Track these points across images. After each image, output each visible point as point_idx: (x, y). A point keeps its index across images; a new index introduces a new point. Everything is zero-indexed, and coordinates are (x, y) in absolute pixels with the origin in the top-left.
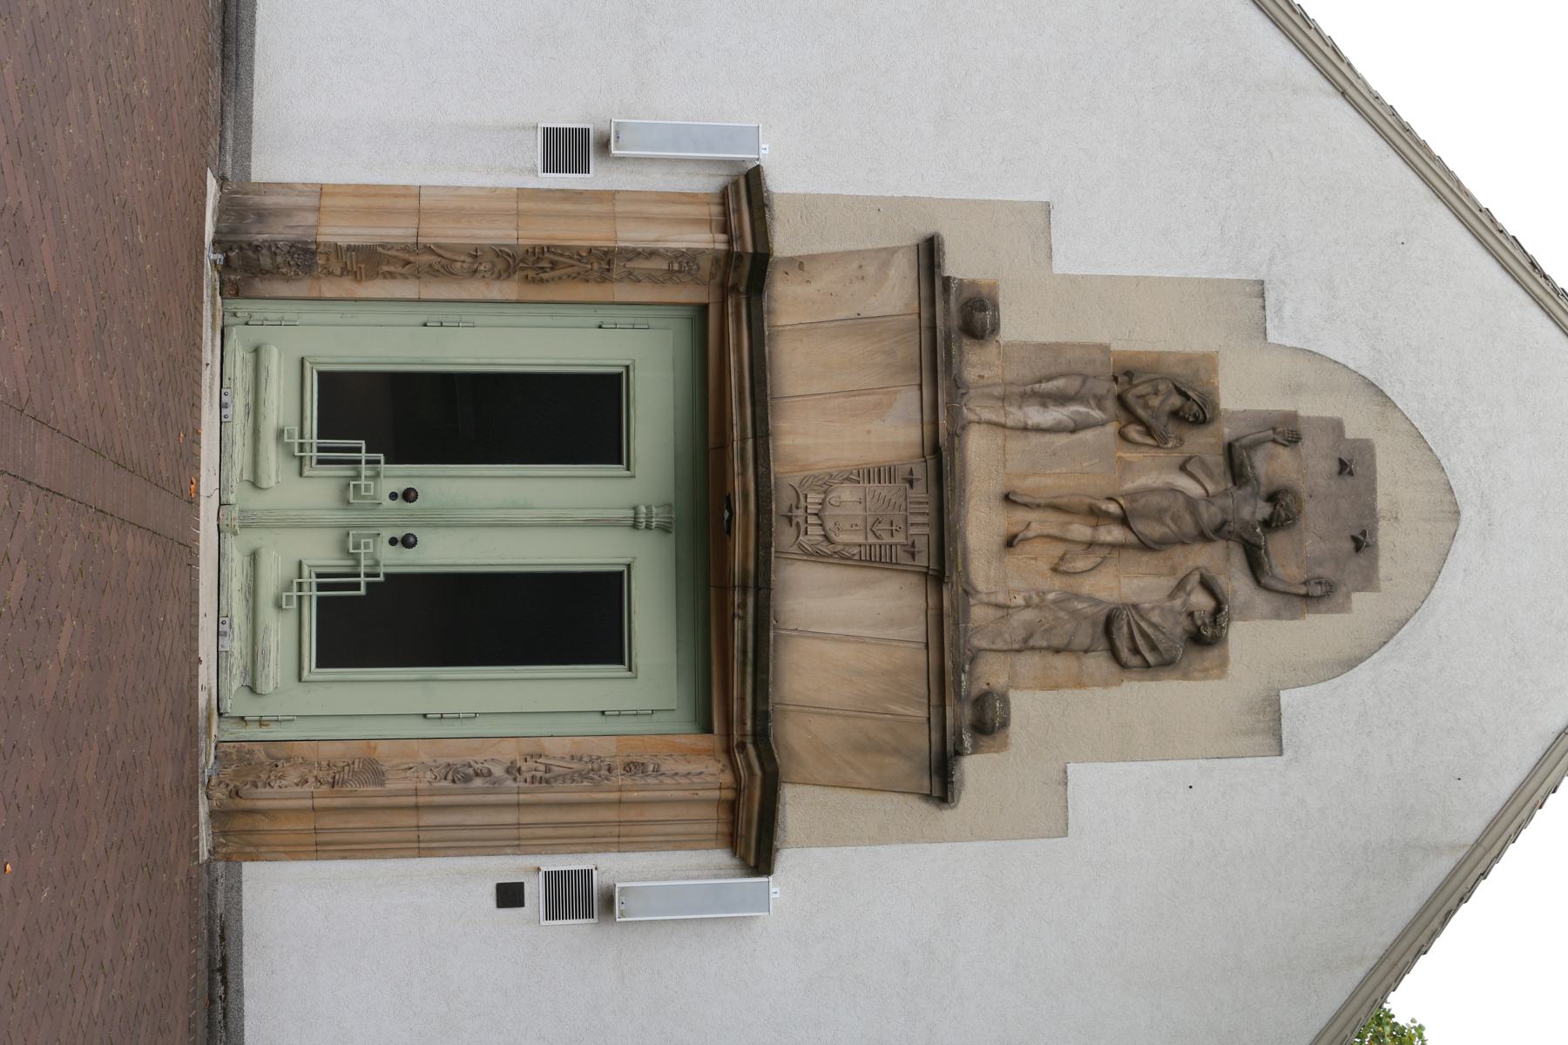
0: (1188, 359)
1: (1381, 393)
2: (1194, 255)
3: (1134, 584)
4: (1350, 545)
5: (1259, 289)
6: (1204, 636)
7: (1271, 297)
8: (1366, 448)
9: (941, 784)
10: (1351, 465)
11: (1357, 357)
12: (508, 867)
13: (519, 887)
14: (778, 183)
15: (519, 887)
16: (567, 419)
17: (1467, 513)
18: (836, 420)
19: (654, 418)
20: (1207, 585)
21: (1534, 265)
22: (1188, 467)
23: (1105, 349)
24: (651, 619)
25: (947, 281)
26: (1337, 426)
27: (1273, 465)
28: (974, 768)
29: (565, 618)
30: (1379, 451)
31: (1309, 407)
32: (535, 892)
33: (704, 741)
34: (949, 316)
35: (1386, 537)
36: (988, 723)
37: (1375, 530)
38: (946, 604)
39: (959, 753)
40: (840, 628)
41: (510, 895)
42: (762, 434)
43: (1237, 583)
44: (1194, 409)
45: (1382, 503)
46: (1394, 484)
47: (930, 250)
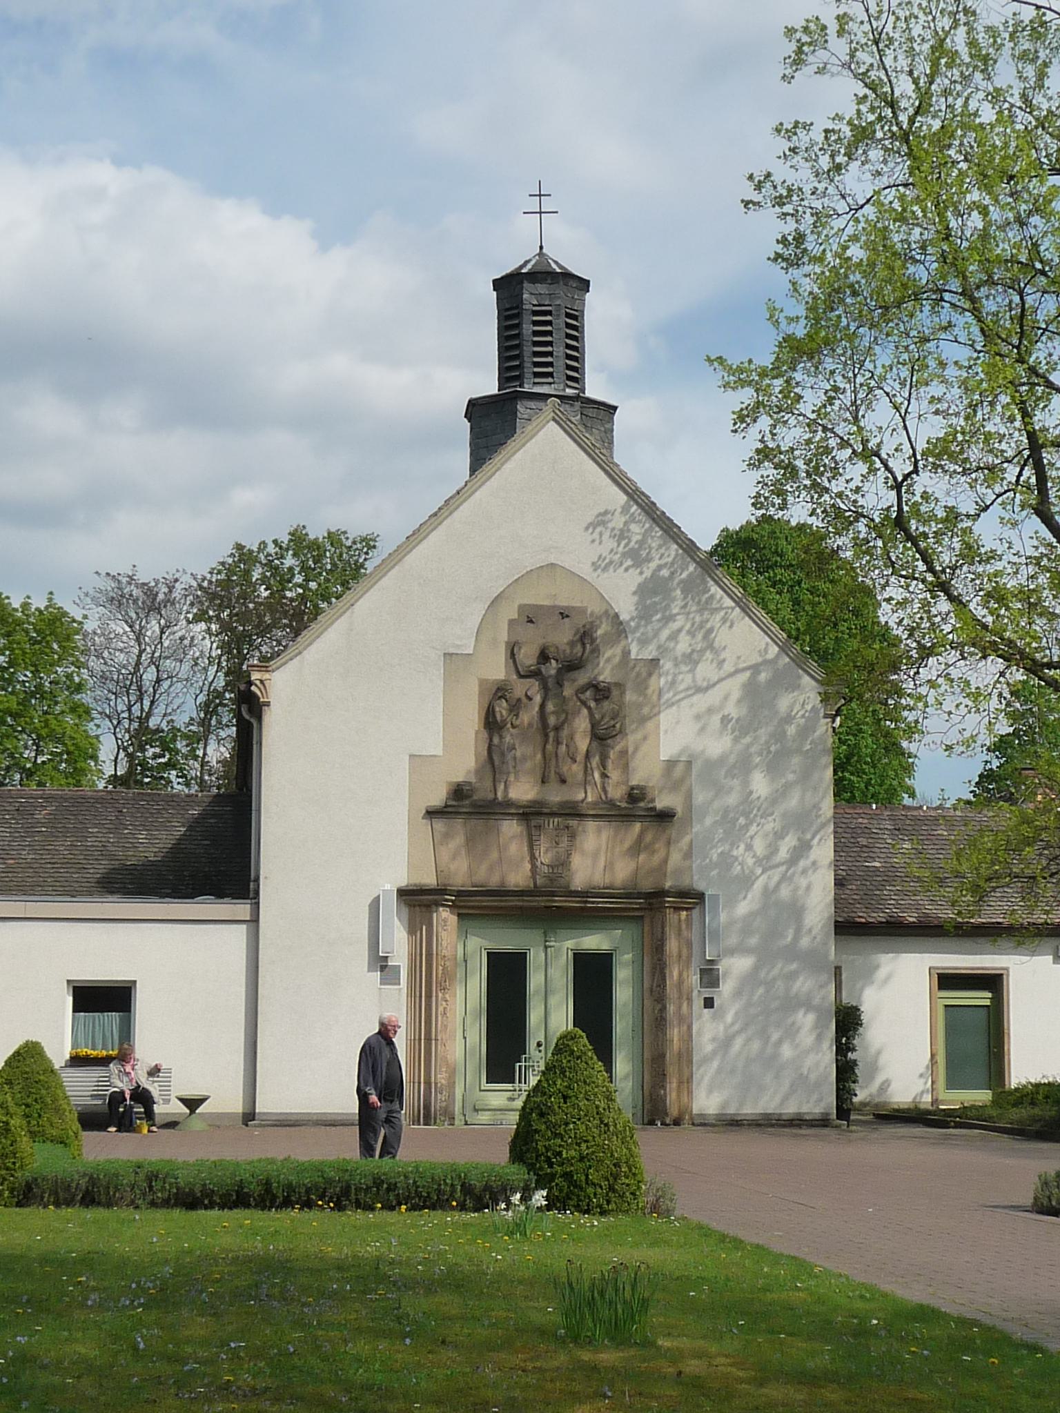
0: (481, 694)
1: (496, 598)
2: (433, 683)
4: (566, 620)
5: (448, 656)
6: (601, 692)
7: (452, 650)
8: (522, 608)
9: (664, 817)
10: (530, 616)
11: (479, 610)
12: (698, 1003)
13: (712, 1006)
14: (403, 882)
15: (712, 1006)
16: (507, 976)
17: (552, 559)
18: (512, 860)
19: (508, 939)
21: (435, 514)
22: (824, 1101)
23: (477, 732)
24: (594, 941)
25: (446, 806)
26: (511, 623)
27: (528, 656)
28: (661, 803)
29: (592, 976)
30: (526, 602)
31: (504, 636)
32: (707, 993)
33: (647, 921)
34: (465, 807)
35: (563, 602)
36: (636, 796)
37: (559, 607)
38: (591, 812)
39: (654, 809)
40: (598, 858)
41: (709, 1003)
43: (582, 678)
44: (500, 691)
45: (546, 603)
46: (539, 596)
47: (431, 814)
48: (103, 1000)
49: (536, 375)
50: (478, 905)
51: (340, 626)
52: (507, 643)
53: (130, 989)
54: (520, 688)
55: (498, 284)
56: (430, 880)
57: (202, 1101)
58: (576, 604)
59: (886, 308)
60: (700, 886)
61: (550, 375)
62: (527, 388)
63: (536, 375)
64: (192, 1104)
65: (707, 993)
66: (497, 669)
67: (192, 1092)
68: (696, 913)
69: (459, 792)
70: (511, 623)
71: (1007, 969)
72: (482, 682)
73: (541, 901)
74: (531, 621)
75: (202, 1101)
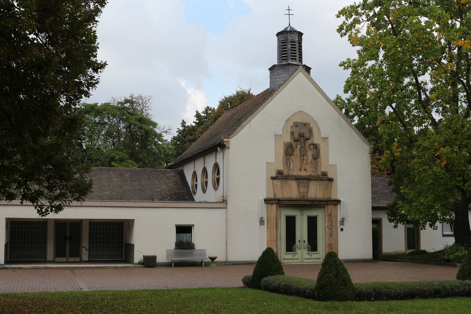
0: (284, 146)
3: (310, 154)
5: (275, 135)
8: (294, 123)
9: (331, 180)
10: (296, 125)
11: (283, 123)
12: (339, 230)
14: (265, 196)
16: (291, 222)
17: (301, 110)
18: (292, 191)
19: (291, 213)
20: (310, 146)
24: (312, 213)
27: (296, 136)
28: (330, 176)
29: (312, 222)
32: (342, 227)
34: (280, 176)
36: (324, 174)
39: (328, 178)
40: (315, 191)
41: (342, 230)
42: (296, 200)
43: (310, 142)
45: (300, 121)
46: (298, 119)
47: (273, 178)
48: (184, 230)
49: (292, 59)
50: (280, 203)
51: (247, 126)
52: (291, 132)
53: (191, 227)
54: (294, 144)
55: (278, 34)
56: (272, 196)
57: (215, 258)
58: (308, 122)
59: (395, 47)
60: (339, 198)
61: (295, 59)
62: (290, 62)
63: (292, 59)
64: (213, 259)
65: (342, 227)
66: (288, 139)
67: (213, 255)
68: (338, 206)
69: (280, 173)
70: (292, 126)
71: (382, 219)
72: (284, 143)
73: (302, 203)
74: (297, 126)
75: (215, 258)
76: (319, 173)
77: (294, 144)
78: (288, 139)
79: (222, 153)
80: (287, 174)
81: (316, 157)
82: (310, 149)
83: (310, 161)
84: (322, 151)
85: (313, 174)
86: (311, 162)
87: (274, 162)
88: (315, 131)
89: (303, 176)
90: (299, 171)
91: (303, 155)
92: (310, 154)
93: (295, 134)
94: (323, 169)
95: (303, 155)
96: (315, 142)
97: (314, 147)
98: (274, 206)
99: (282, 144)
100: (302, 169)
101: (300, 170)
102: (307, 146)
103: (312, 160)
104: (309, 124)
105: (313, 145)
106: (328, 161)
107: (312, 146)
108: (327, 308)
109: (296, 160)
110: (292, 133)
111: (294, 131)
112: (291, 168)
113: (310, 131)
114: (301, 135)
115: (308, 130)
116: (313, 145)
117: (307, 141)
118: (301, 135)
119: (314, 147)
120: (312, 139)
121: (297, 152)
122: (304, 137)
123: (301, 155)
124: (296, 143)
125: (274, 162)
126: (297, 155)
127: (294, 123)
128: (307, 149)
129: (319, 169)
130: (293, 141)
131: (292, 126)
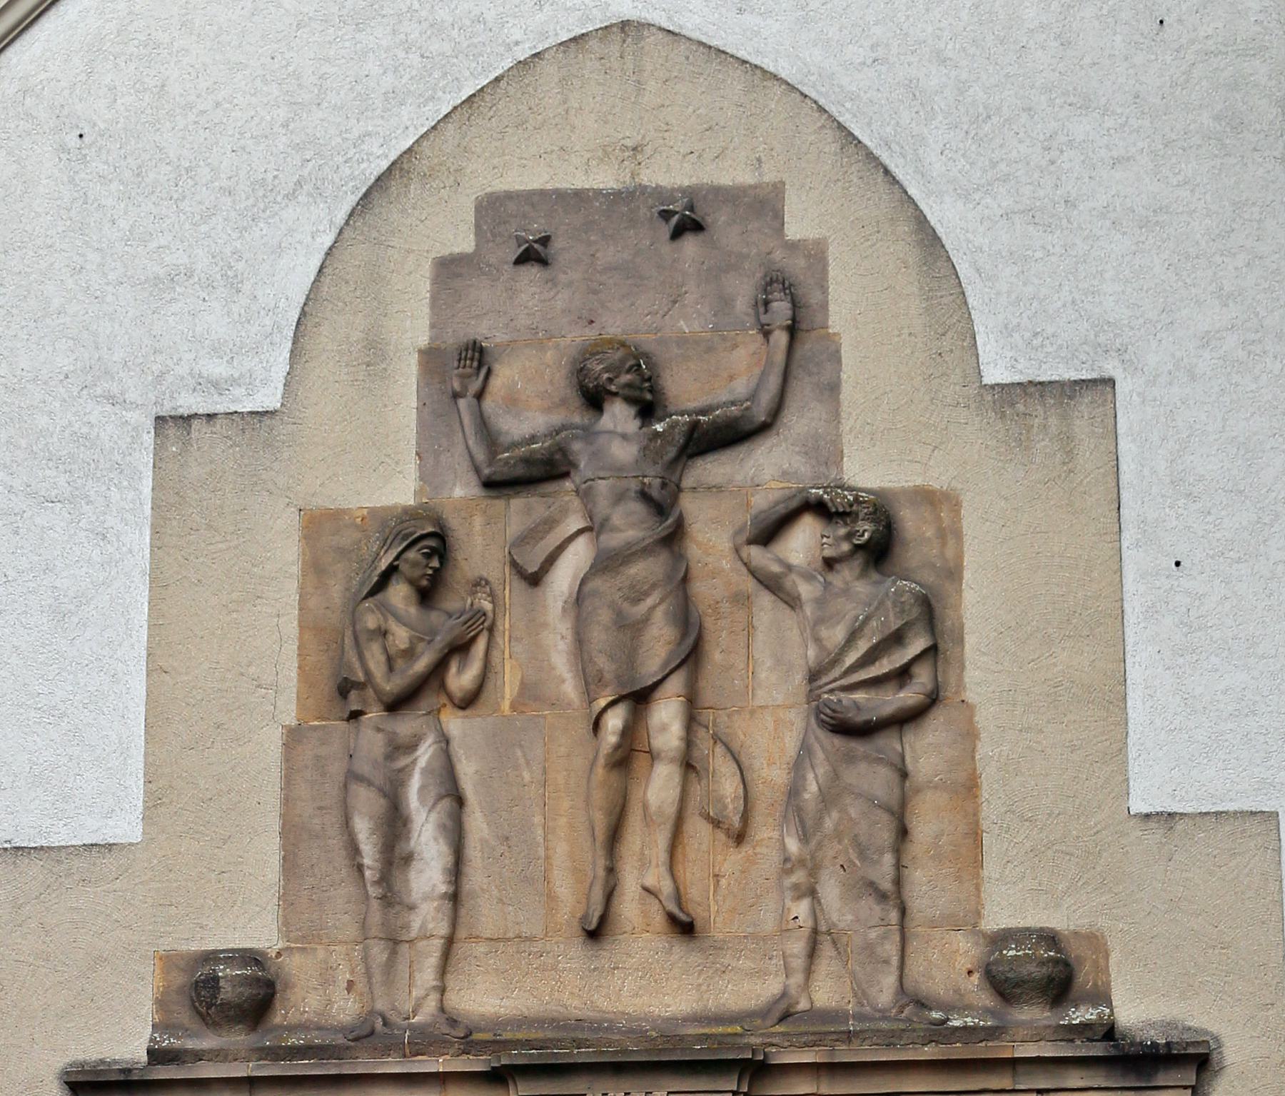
0: (315, 568)
3: (768, 677)
8: (492, 209)
11: (315, 227)
20: (770, 531)
27: (528, 403)
39: (1109, 1032)
52: (431, 358)
70: (449, 270)
72: (318, 525)
76: (948, 967)
77: (483, 540)
78: (387, 467)
79: (810, 663)
80: (346, 1009)
81: (886, 701)
82: (772, 584)
83: (771, 774)
84: (980, 612)
85: (827, 992)
86: (794, 792)
87: (126, 827)
88: (859, 305)
89: (669, 1033)
90: (572, 955)
91: (656, 676)
92: (768, 677)
93: (505, 376)
94: (1014, 902)
95: (656, 676)
96: (865, 471)
97: (833, 539)
98: (443, 888)
99: (286, 553)
100: (629, 907)
101: (595, 933)
102: (712, 535)
103: (805, 749)
104: (764, 205)
105: (820, 509)
106: (1116, 753)
107: (803, 542)
108: (625, 1052)
109: (518, 749)
110: (464, 367)
111: (488, 331)
112: (427, 917)
113: (790, 312)
114: (617, 380)
115: (743, 291)
116: (820, 509)
117: (713, 469)
118: (617, 380)
119: (833, 539)
120: (801, 420)
121: (541, 644)
122: (647, 410)
123: (590, 682)
124: (519, 511)
125: (126, 827)
126: (530, 694)
127: (492, 209)
128: (705, 590)
129: (928, 888)
130: (461, 488)
131: (449, 270)
